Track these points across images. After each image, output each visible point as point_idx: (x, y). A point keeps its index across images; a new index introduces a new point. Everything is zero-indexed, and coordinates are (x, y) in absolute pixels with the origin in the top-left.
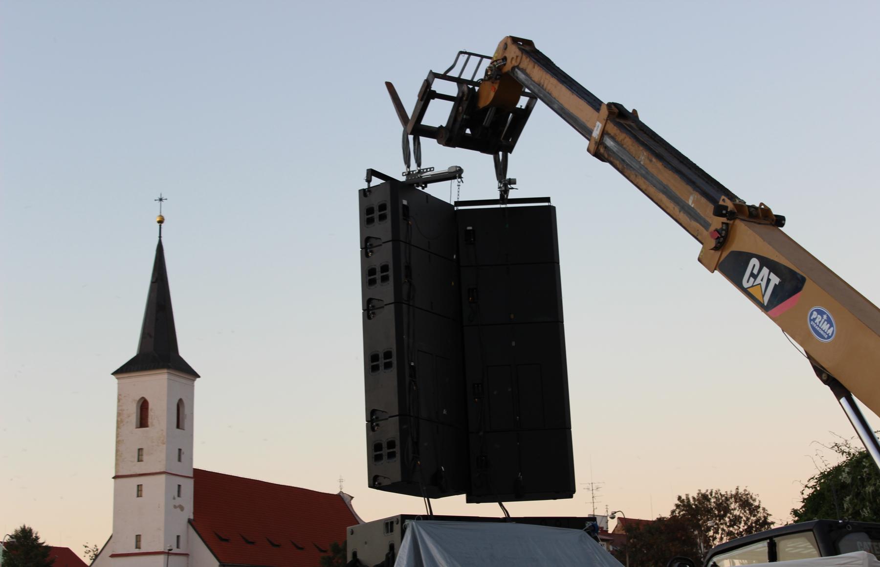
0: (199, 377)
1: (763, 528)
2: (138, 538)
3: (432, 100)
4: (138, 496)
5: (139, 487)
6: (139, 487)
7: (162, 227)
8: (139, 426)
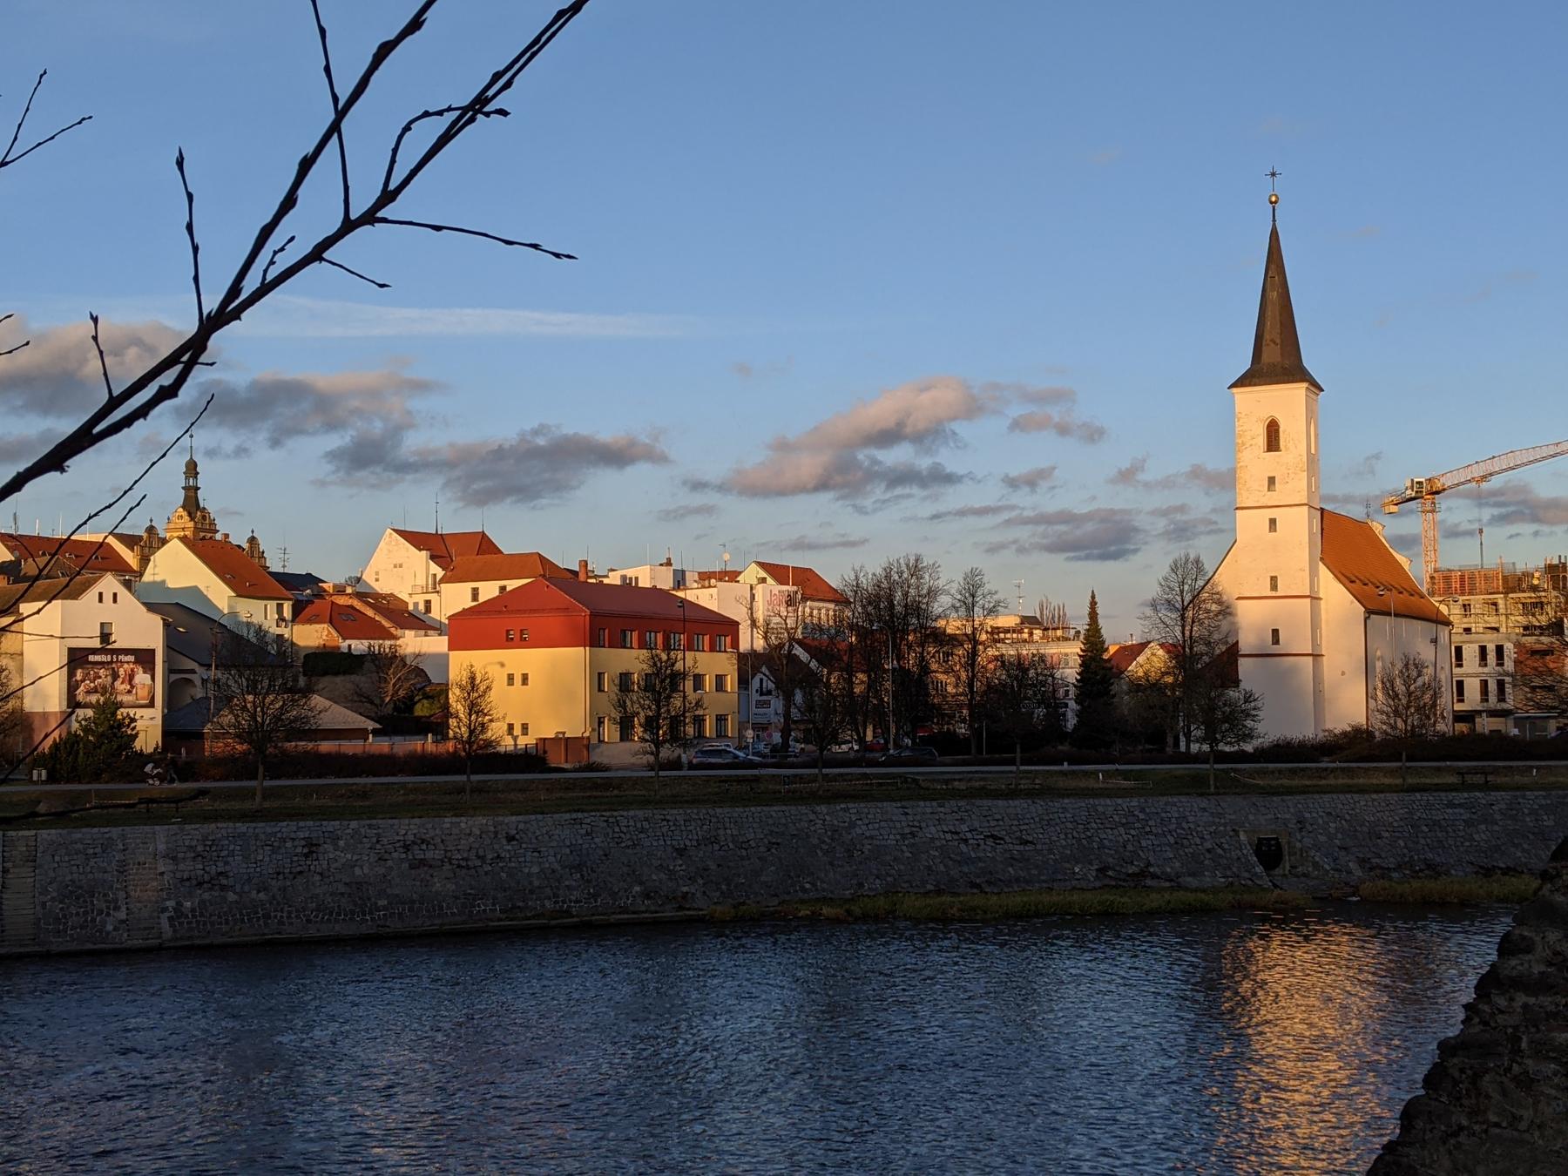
0: (1323, 390)
2: (1274, 579)
5: (1273, 522)
6: (1273, 522)
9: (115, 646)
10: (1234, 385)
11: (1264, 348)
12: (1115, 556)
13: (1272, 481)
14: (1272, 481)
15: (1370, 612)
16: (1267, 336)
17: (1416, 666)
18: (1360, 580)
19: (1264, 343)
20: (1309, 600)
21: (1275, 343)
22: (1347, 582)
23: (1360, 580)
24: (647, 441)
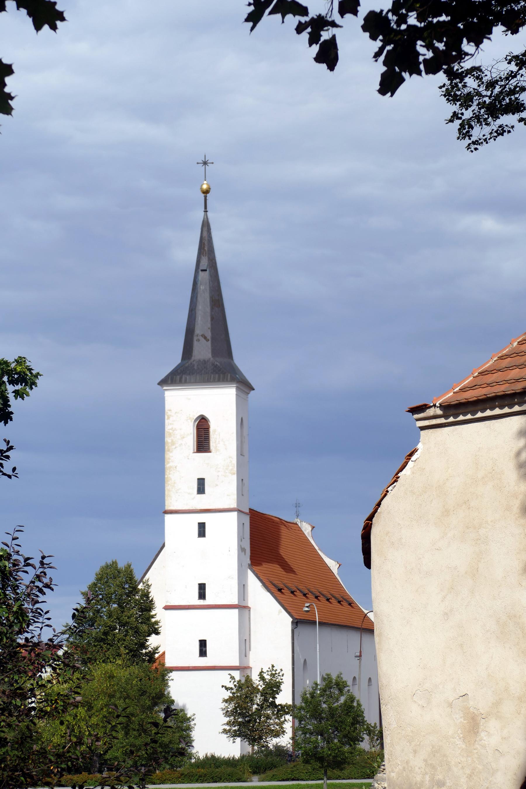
0: (254, 389)
1: (358, 739)
2: (202, 587)
3: (292, 620)
4: (204, 585)
5: (203, 653)
6: (203, 653)
7: (208, 198)
8: (195, 451)
9: (138, 581)
10: (164, 382)
11: (195, 343)
12: (245, 550)
13: (201, 483)
14: (201, 483)
15: (296, 623)
16: (198, 331)
17: (337, 684)
18: (323, 595)
19: (195, 338)
20: (236, 611)
21: (205, 338)
22: (275, 590)
23: (323, 595)
24: (200, 279)
